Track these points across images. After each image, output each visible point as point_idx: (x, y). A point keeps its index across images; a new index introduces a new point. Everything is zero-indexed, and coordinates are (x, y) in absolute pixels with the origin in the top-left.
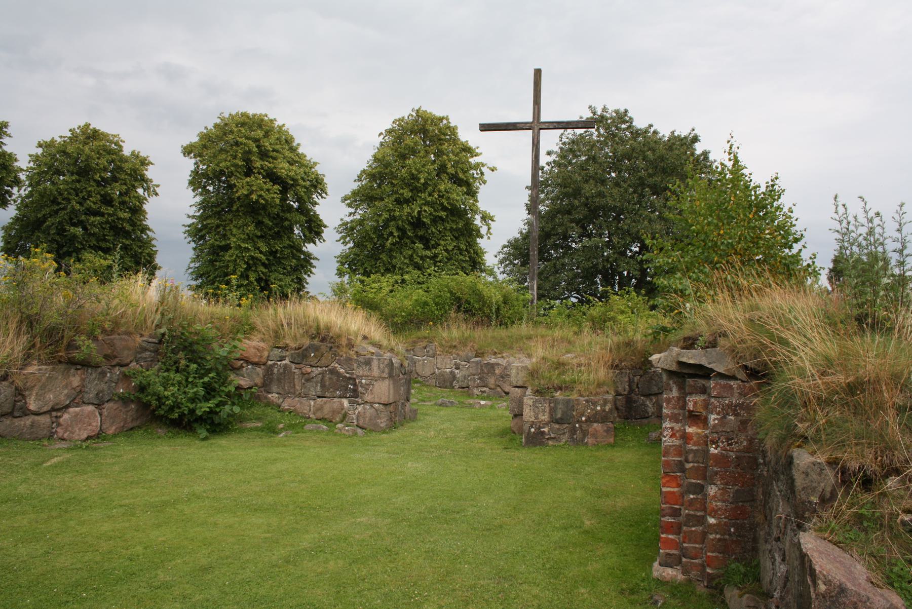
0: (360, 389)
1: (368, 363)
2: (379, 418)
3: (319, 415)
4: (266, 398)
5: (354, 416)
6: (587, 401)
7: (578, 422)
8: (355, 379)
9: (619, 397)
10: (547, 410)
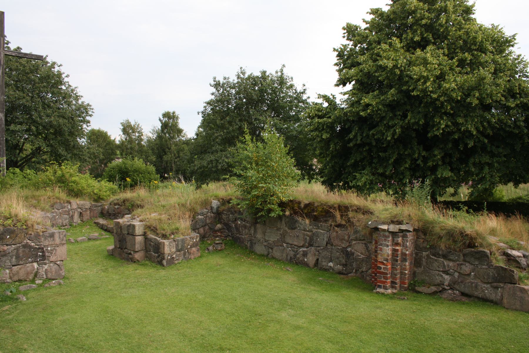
0: (47, 254)
1: (52, 235)
6: (190, 238)
8: (43, 248)
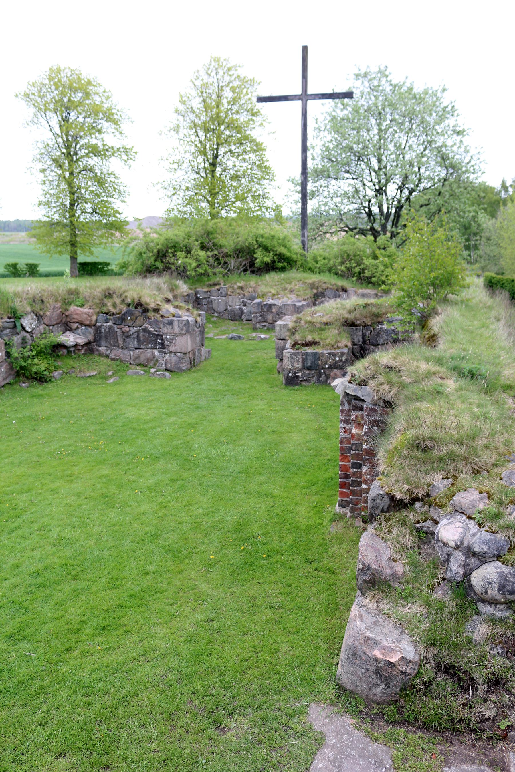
0: (166, 343)
1: (171, 323)
2: (182, 363)
3: (137, 361)
4: (98, 350)
5: (163, 362)
7: (323, 368)
8: (162, 336)
9: (356, 347)
10: (301, 360)
